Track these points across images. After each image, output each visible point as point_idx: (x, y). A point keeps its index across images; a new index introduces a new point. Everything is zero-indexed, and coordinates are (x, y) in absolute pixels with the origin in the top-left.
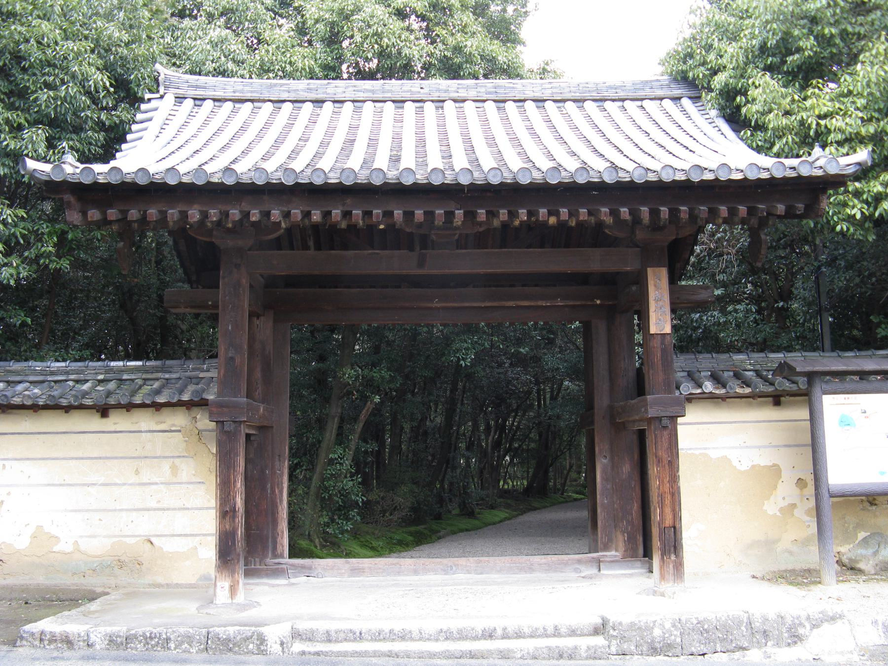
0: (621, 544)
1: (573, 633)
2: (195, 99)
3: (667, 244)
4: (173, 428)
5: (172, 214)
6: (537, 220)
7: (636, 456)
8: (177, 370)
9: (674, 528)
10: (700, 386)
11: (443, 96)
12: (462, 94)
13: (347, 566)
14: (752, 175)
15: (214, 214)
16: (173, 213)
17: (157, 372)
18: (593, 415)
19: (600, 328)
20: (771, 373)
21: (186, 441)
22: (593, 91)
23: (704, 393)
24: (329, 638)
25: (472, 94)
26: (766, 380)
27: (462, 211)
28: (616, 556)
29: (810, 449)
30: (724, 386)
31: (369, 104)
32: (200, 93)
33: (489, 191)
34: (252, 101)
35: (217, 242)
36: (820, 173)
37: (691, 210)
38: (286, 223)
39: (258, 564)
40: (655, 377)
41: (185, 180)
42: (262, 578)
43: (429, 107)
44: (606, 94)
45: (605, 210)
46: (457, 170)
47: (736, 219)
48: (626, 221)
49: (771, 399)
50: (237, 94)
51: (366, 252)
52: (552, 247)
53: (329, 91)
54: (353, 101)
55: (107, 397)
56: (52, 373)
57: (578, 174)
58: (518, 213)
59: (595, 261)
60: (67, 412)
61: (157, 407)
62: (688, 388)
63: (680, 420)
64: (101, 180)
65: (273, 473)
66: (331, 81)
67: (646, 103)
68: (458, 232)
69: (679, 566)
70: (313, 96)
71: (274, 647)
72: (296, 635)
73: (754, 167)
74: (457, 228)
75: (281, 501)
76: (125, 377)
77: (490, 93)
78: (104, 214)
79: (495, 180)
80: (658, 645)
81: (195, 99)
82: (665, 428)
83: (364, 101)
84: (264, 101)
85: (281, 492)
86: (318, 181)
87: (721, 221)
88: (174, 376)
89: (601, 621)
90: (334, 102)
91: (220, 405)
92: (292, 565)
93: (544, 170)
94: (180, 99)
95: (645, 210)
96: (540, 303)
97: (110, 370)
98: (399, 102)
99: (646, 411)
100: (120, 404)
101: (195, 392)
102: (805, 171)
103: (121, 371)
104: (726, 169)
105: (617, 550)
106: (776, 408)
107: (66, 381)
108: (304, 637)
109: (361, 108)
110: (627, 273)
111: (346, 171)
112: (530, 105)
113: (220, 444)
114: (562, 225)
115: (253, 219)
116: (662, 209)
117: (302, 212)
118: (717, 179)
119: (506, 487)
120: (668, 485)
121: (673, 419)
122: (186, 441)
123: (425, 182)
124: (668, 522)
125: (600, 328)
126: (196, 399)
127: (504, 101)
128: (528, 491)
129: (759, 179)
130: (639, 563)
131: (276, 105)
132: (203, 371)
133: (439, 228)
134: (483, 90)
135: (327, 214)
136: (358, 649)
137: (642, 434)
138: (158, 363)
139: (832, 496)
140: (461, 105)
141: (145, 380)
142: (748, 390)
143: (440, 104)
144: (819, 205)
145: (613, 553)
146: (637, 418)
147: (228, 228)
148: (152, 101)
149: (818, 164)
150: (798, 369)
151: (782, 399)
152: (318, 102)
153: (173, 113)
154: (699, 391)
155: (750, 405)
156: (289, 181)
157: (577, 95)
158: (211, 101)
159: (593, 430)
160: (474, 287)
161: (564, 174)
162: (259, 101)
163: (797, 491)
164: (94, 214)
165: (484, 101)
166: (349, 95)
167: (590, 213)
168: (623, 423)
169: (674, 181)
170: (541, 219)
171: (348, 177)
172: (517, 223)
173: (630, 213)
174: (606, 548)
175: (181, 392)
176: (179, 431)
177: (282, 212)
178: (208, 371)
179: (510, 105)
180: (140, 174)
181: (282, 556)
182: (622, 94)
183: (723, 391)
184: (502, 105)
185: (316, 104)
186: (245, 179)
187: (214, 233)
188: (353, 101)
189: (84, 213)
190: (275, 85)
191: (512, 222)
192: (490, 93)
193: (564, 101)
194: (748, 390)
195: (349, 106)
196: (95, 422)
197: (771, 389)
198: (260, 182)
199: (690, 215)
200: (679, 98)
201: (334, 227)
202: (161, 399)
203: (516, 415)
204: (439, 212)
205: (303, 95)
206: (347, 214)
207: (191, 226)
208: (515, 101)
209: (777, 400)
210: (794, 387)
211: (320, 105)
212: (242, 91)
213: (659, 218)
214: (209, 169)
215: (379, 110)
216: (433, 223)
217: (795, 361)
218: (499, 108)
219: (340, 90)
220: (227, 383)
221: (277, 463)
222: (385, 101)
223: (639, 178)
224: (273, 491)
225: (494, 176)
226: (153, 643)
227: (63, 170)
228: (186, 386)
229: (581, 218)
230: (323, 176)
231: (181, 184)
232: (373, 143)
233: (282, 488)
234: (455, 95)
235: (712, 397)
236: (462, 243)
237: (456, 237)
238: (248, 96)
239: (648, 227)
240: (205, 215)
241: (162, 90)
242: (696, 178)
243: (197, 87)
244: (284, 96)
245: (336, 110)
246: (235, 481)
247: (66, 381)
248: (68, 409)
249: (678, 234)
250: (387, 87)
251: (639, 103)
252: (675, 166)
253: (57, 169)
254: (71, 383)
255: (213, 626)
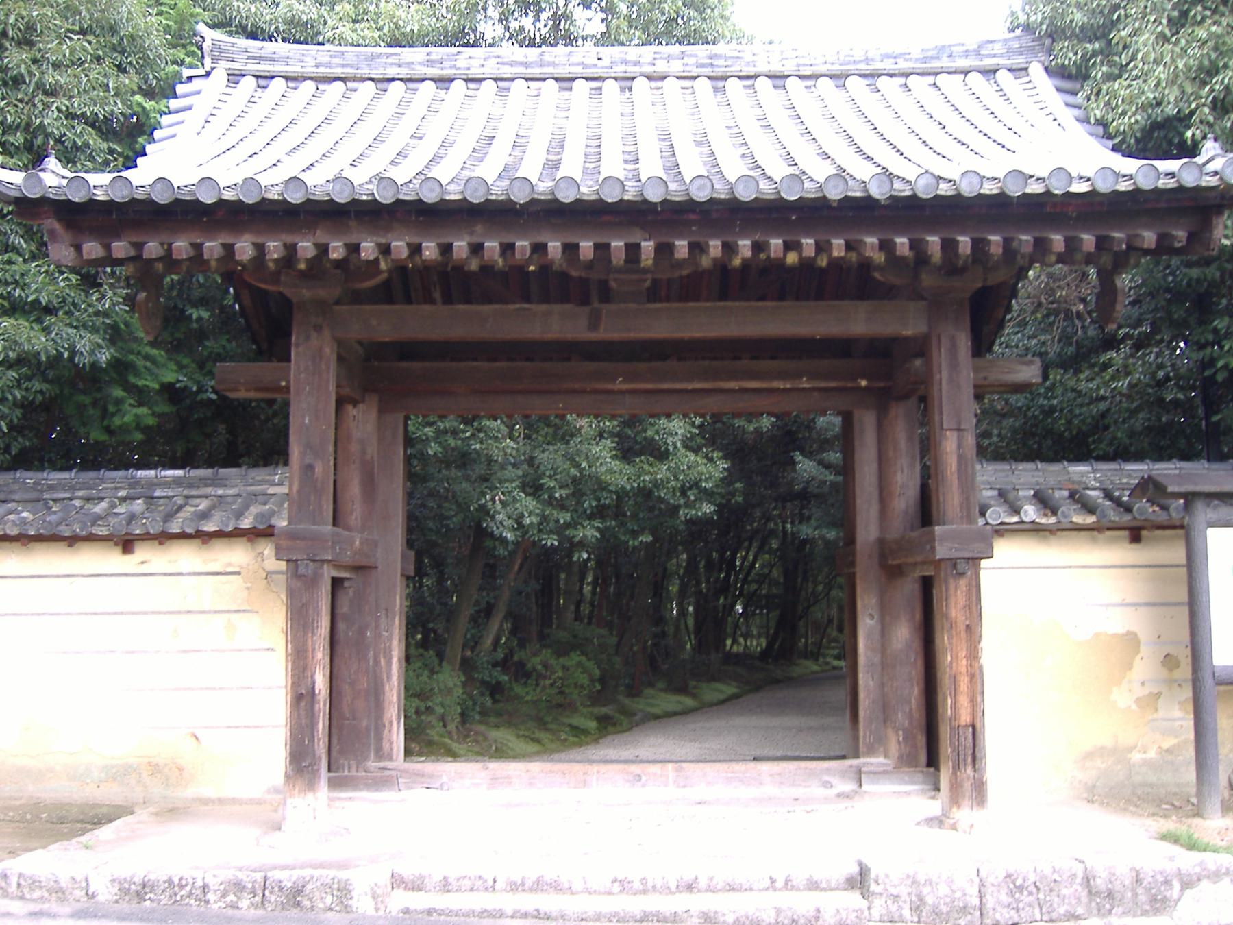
0: (894, 748)
1: (813, 886)
2: (257, 77)
3: (968, 295)
4: (229, 570)
5: (211, 249)
6: (768, 257)
7: (918, 616)
8: (236, 482)
9: (974, 727)
10: (1017, 511)
11: (632, 70)
12: (661, 67)
13: (484, 774)
14: (1104, 187)
15: (274, 248)
16: (212, 247)
17: (206, 486)
18: (853, 554)
19: (867, 421)
20: (1127, 493)
21: (248, 588)
22: (860, 62)
23: (1022, 522)
24: (446, 886)
25: (676, 67)
26: (1118, 502)
27: (652, 243)
28: (884, 765)
29: (1186, 610)
30: (1054, 513)
31: (520, 83)
32: (265, 67)
33: (694, 212)
34: (344, 80)
35: (288, 292)
36: (1213, 181)
37: (1007, 242)
38: (386, 262)
39: (354, 769)
40: (950, 498)
41: (228, 195)
42: (360, 790)
43: (611, 87)
44: (878, 65)
45: (871, 240)
46: (643, 180)
47: (1078, 257)
48: (903, 258)
49: (1126, 533)
50: (322, 70)
51: (512, 307)
52: (797, 299)
53: (459, 64)
54: (496, 80)
55: (129, 523)
56: (51, 487)
57: (831, 184)
58: (708, 245)
59: (857, 321)
60: (70, 546)
61: (203, 537)
62: (998, 515)
63: (984, 563)
64: (101, 196)
65: (378, 636)
66: (461, 49)
67: (942, 80)
68: (649, 276)
69: (979, 792)
70: (434, 71)
71: (362, 904)
72: (397, 882)
73: (1109, 172)
74: (645, 271)
75: (389, 678)
76: (157, 494)
77: (703, 66)
78: (108, 247)
79: (701, 196)
80: (944, 909)
81: (257, 77)
82: (962, 574)
83: (513, 79)
84: (363, 80)
85: (389, 663)
86: (430, 197)
87: (1053, 258)
88: (231, 492)
89: (856, 869)
90: (467, 80)
91: (291, 535)
92: (406, 771)
93: (778, 179)
94: (235, 77)
95: (933, 240)
96: (777, 384)
97: (135, 484)
98: (566, 81)
99: (933, 549)
100: (148, 533)
101: (260, 516)
102: (1190, 179)
103: (152, 485)
104: (1063, 175)
105: (886, 756)
106: (1134, 546)
107: (70, 499)
108: (410, 886)
109: (508, 89)
110: (907, 339)
111: (473, 182)
112: (763, 84)
113: (291, 593)
114: (807, 265)
115: (334, 256)
116: (961, 239)
117: (408, 244)
118: (1048, 193)
119: (735, 648)
120: (964, 662)
121: (974, 561)
122: (248, 588)
123: (593, 197)
124: (965, 718)
125: (867, 421)
126: (261, 527)
127: (725, 78)
128: (765, 655)
129: (1116, 192)
130: (920, 775)
131: (380, 85)
132: (273, 484)
133: (619, 270)
134: (692, 61)
135: (446, 249)
136: (489, 907)
137: (927, 585)
138: (208, 472)
139: (1220, 683)
140: (659, 84)
141: (187, 497)
142: (1091, 519)
143: (628, 83)
144: (1211, 232)
145: (881, 760)
146: (919, 558)
147: (300, 271)
148: (194, 80)
149: (1211, 167)
150: (1170, 489)
151: (1144, 533)
152: (444, 82)
153: (224, 98)
154: (1015, 519)
155: (1094, 540)
156: (386, 198)
157: (836, 68)
158: (283, 80)
159: (854, 574)
160: (679, 359)
161: (807, 184)
162: (354, 79)
163: (1164, 673)
164: (92, 249)
165: (695, 78)
166: (491, 69)
167: (849, 246)
168: (899, 566)
169: (980, 195)
170: (772, 255)
171: (476, 190)
172: (737, 262)
173: (911, 248)
174: (871, 751)
175: (239, 515)
176: (238, 573)
177: (379, 245)
178: (280, 484)
179: (733, 85)
180: (159, 186)
181: (390, 758)
182: (903, 65)
183: (1053, 520)
184: (721, 84)
185: (439, 84)
186: (320, 195)
187: (283, 278)
188: (496, 80)
189: (78, 248)
190: (379, 55)
191: (730, 260)
192: (703, 66)
193: (815, 77)
194: (1091, 519)
195: (489, 86)
196: (110, 560)
197: (1127, 518)
198: (342, 199)
199: (1004, 247)
200: (995, 71)
201: (459, 268)
202: (210, 527)
203: (750, 544)
204: (617, 244)
205: (421, 71)
206: (477, 249)
207: (244, 266)
208: (740, 78)
209: (1135, 535)
210: (1162, 517)
211: (446, 85)
212: (328, 65)
213: (957, 254)
214: (264, 180)
215: (535, 93)
216: (610, 261)
217: (1166, 475)
218: (715, 89)
219: (473, 62)
220: (300, 505)
221: (383, 621)
222: (544, 80)
223: (924, 190)
224: (377, 662)
225: (699, 189)
226: (183, 892)
227: (40, 180)
228: (247, 507)
229: (835, 254)
230: (438, 189)
231: (221, 202)
232: (519, 143)
233: (391, 658)
234: (648, 69)
235: (1035, 530)
236: (657, 292)
237: (648, 284)
238: (339, 71)
239: (940, 268)
240: (260, 248)
241: (207, 61)
242: (1014, 191)
243: (261, 59)
244: (392, 72)
245: (470, 93)
246: (313, 650)
247: (70, 499)
248: (73, 541)
249: (986, 280)
250: (547, 58)
251: (931, 79)
252: (982, 174)
253: (34, 179)
254: (77, 503)
255: (275, 868)
